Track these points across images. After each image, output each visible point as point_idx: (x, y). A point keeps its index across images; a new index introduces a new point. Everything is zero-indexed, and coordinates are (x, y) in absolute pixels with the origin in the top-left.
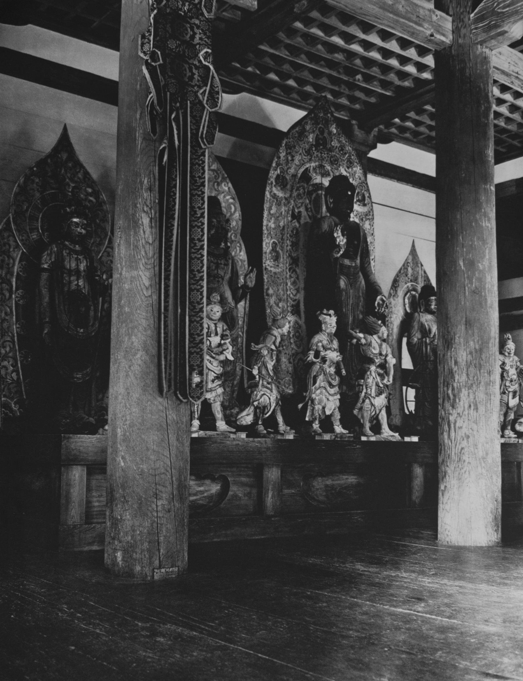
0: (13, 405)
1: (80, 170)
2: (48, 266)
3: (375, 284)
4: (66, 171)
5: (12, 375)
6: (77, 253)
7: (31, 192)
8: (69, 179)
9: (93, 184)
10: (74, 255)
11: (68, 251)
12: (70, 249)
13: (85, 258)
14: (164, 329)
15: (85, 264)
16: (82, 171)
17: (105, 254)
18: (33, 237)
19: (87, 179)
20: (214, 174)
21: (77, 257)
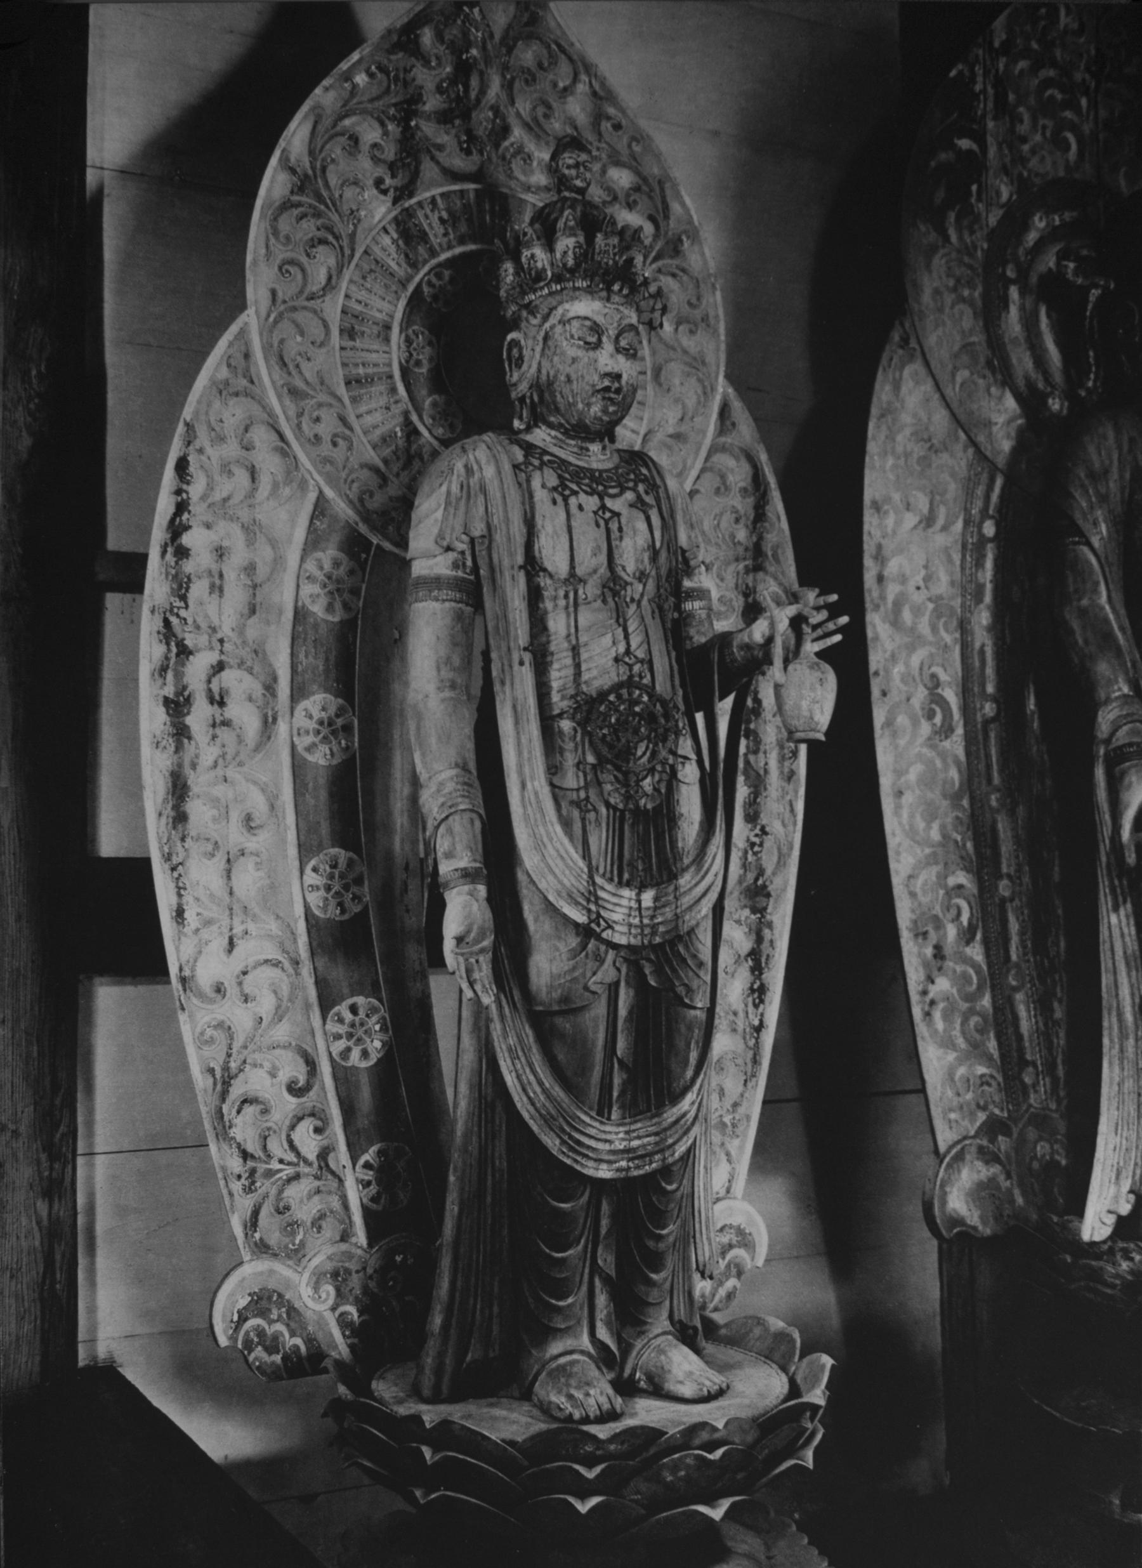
0: (306, 1292)
1: (576, 79)
2: (455, 566)
3: (760, 678)
4: (508, 86)
5: (296, 1136)
6: (596, 482)
7: (349, 192)
8: (527, 126)
9: (637, 148)
10: (583, 497)
11: (553, 481)
12: (561, 465)
13: (639, 504)
14: (657, 854)
15: (642, 539)
16: (582, 88)
17: (709, 483)
18: (369, 420)
19: (606, 126)
20: (446, 234)
21: (603, 507)
